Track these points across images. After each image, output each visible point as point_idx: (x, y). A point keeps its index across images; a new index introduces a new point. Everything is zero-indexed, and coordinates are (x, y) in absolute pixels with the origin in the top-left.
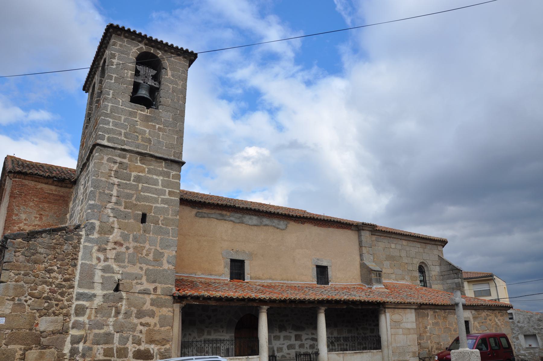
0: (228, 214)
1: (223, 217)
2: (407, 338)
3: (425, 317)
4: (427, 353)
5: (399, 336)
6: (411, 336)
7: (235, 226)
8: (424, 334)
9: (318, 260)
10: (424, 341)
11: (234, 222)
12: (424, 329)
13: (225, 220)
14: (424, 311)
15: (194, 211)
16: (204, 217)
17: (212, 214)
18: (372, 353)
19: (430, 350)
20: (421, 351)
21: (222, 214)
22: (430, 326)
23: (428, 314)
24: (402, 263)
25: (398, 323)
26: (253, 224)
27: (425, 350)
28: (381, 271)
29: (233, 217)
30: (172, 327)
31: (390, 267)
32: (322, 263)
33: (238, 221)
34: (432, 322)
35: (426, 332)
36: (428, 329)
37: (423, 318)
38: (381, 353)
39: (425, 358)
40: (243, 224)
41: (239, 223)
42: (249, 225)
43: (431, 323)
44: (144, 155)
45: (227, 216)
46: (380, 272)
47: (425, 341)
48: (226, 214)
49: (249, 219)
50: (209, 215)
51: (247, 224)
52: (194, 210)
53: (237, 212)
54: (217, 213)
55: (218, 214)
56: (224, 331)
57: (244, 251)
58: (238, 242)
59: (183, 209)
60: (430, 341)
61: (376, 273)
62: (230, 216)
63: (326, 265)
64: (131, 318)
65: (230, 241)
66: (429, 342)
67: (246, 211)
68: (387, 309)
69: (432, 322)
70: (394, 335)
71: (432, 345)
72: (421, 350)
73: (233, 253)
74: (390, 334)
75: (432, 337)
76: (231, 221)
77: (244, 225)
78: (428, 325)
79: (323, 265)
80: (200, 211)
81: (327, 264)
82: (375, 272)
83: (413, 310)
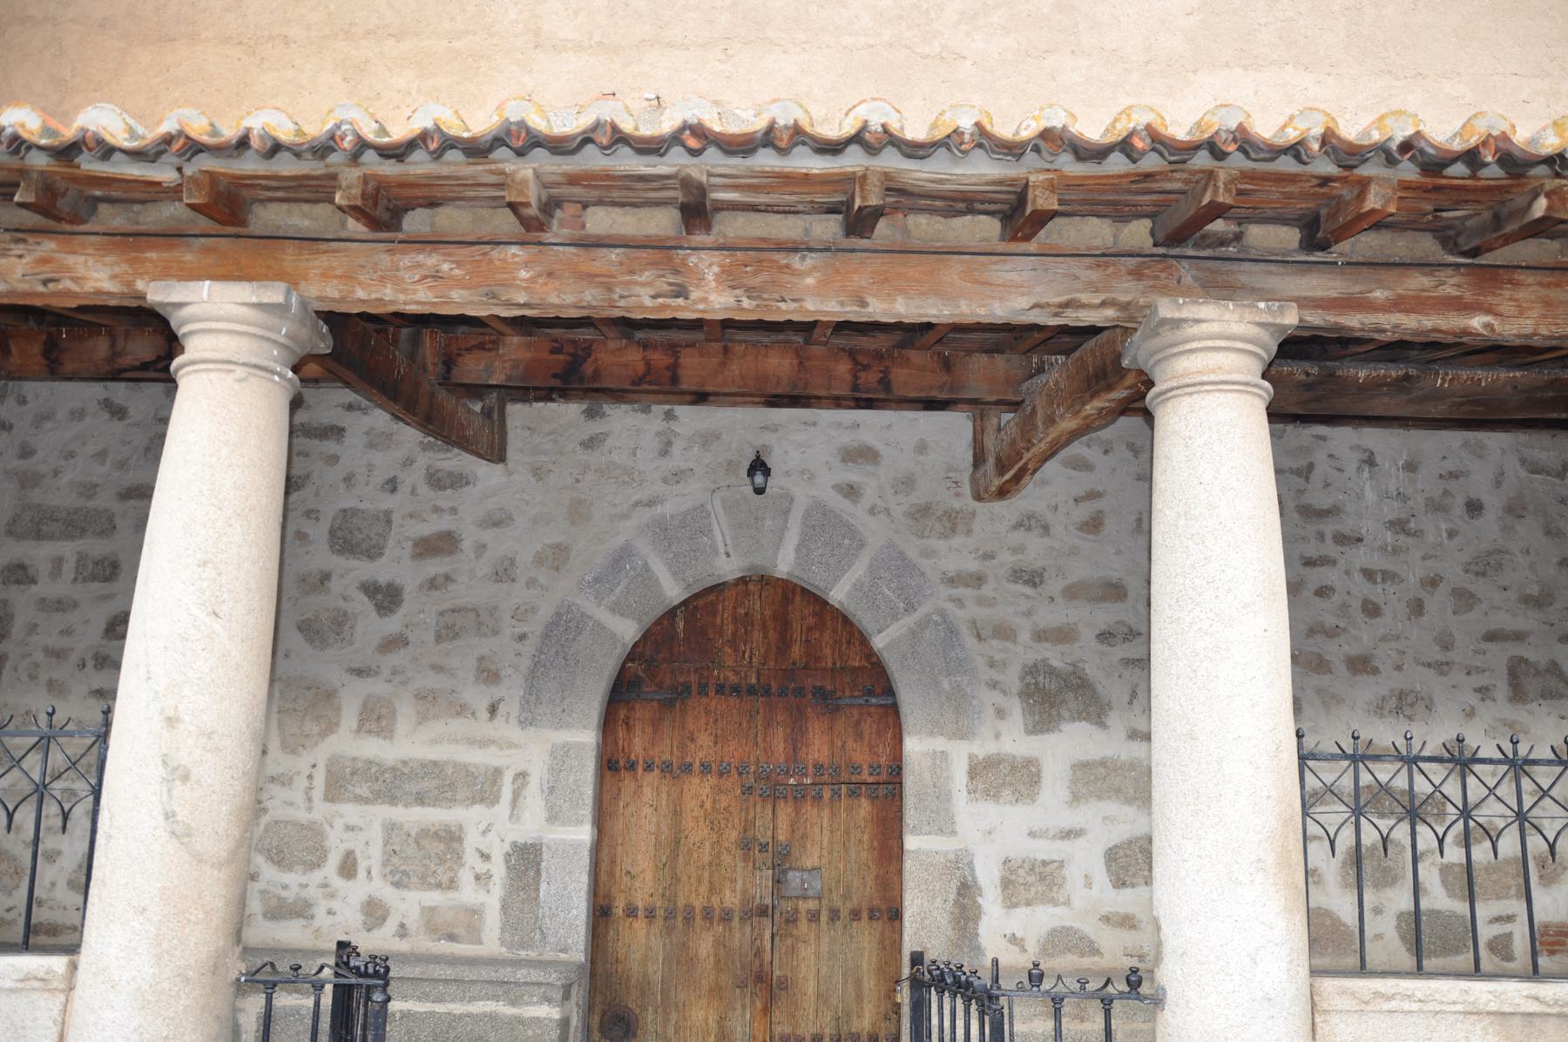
58: (670, 45)
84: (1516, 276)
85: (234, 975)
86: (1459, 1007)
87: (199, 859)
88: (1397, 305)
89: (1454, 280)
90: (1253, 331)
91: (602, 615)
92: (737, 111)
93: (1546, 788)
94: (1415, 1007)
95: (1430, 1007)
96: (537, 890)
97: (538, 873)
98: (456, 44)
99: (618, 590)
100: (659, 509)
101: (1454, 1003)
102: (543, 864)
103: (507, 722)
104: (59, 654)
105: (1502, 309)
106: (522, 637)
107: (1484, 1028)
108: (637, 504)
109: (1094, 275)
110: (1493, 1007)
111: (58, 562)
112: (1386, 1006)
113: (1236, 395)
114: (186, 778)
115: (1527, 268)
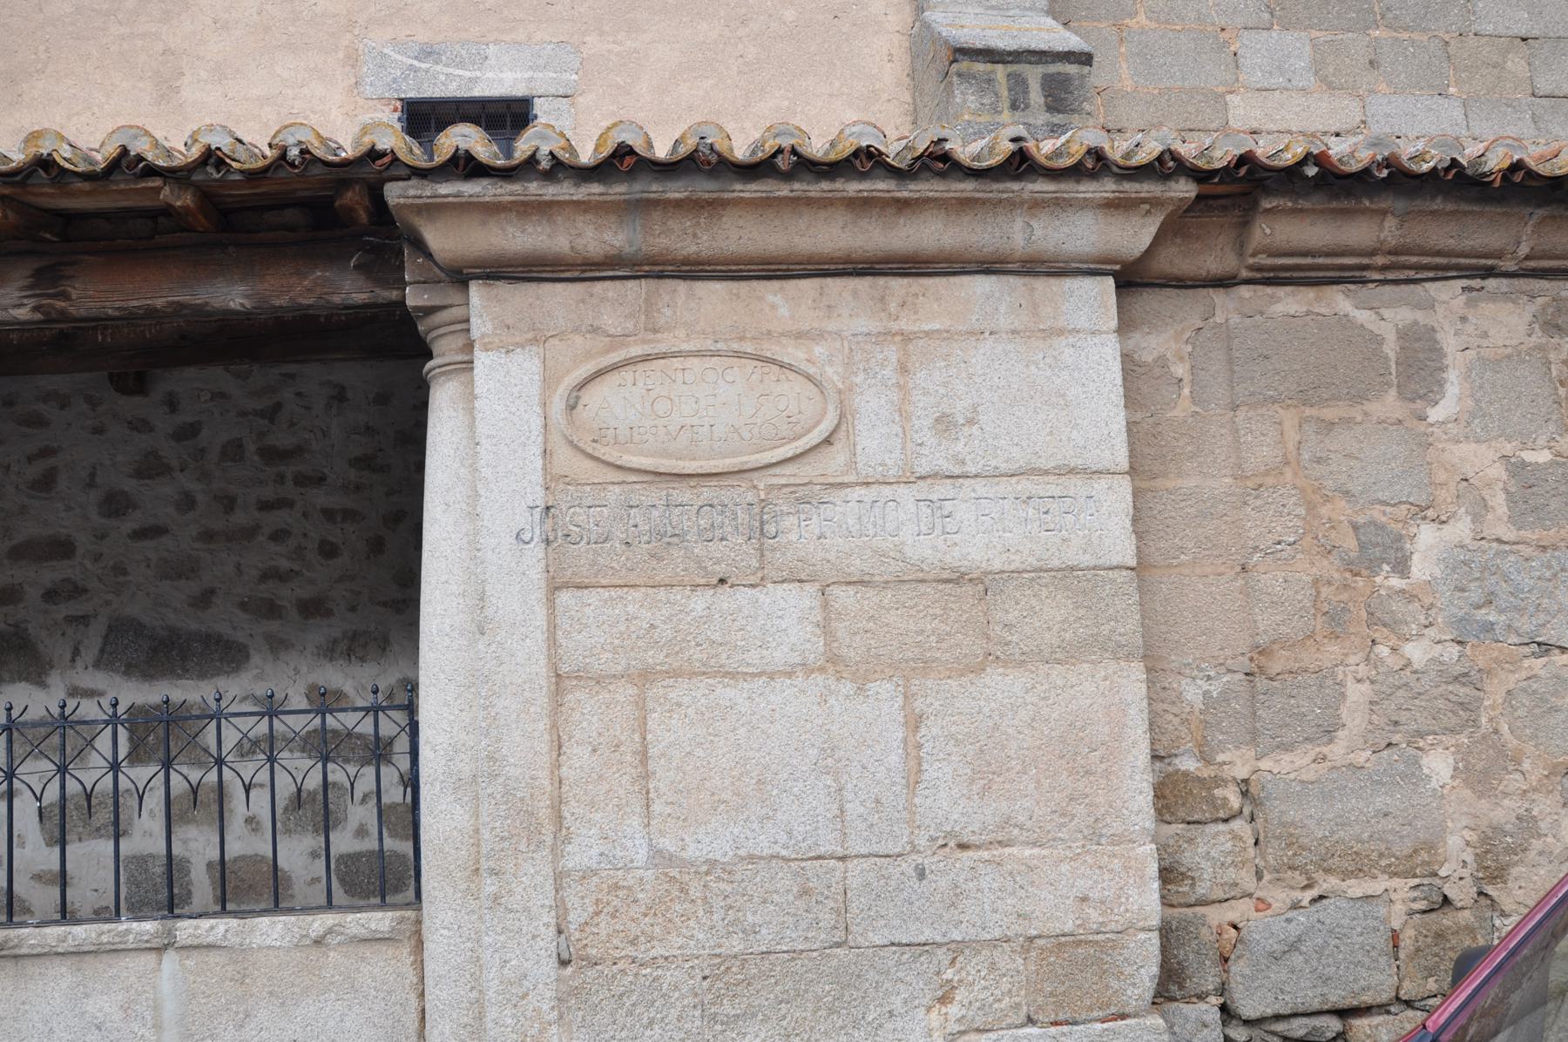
2: (914, 722)
3: (1359, 398)
4: (1395, 937)
5: (727, 693)
6: (1001, 685)
8: (1333, 650)
9: (427, 53)
10: (1336, 751)
12: (1329, 568)
14: (1339, 301)
18: (214, 958)
19: (1461, 893)
20: (1262, 905)
22: (1461, 529)
23: (1437, 351)
24: (1472, 41)
25: (741, 494)
27: (1357, 888)
28: (1085, 59)
31: (1324, 80)
32: (472, 80)
34: (1517, 469)
35: (1373, 620)
36: (1422, 568)
37: (1329, 413)
38: (389, 967)
39: (1343, 1013)
43: (1498, 472)
46: (1071, 69)
47: (1362, 757)
60: (1463, 754)
61: (1018, 83)
63: (519, 91)
64: (1139, 608)
66: (1439, 765)
68: (502, 288)
69: (1517, 469)
70: (625, 692)
71: (1504, 812)
72: (1279, 897)
74: (540, 667)
75: (1494, 693)
78: (1421, 511)
79: (477, 92)
81: (531, 79)
82: (1000, 71)
83: (1088, 283)
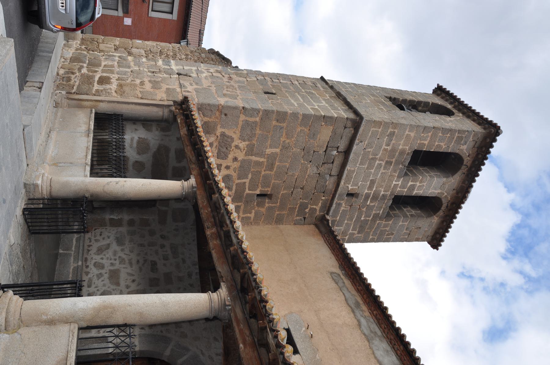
0: (367, 314)
1: (355, 307)
7: (353, 328)
11: (359, 325)
13: (353, 312)
15: (337, 270)
16: (337, 283)
17: (350, 292)
21: (360, 305)
26: (381, 359)
29: (367, 322)
30: (141, 98)
33: (367, 332)
40: (366, 342)
41: (364, 334)
42: (373, 353)
44: (340, 97)
45: (361, 313)
48: (365, 311)
49: (383, 348)
50: (345, 289)
51: (371, 348)
52: (339, 270)
53: (379, 324)
54: (356, 298)
55: (356, 299)
56: (142, 330)
57: (318, 350)
58: (329, 337)
59: (331, 258)
62: (365, 317)
65: (322, 323)
67: (392, 338)
73: (302, 331)
76: (359, 321)
77: (366, 343)
80: (342, 277)
84: (255, 351)
85: (86, 195)
86: (69, 349)
87: (104, 186)
88: (241, 331)
89: (250, 339)
90: (223, 298)
91: (170, 348)
92: (317, 355)
93: (121, 341)
94: (70, 340)
95: (70, 343)
96: (96, 343)
97: (101, 343)
98: (309, 297)
99: (178, 350)
100: (201, 355)
101: (70, 348)
102: (103, 344)
103: (139, 332)
104: (146, 254)
105: (246, 349)
106: (162, 332)
107: (63, 355)
108: (202, 351)
109: (229, 279)
110: (69, 356)
111: (166, 251)
112: (71, 335)
113: (208, 298)
114: (117, 183)
115: (258, 353)
